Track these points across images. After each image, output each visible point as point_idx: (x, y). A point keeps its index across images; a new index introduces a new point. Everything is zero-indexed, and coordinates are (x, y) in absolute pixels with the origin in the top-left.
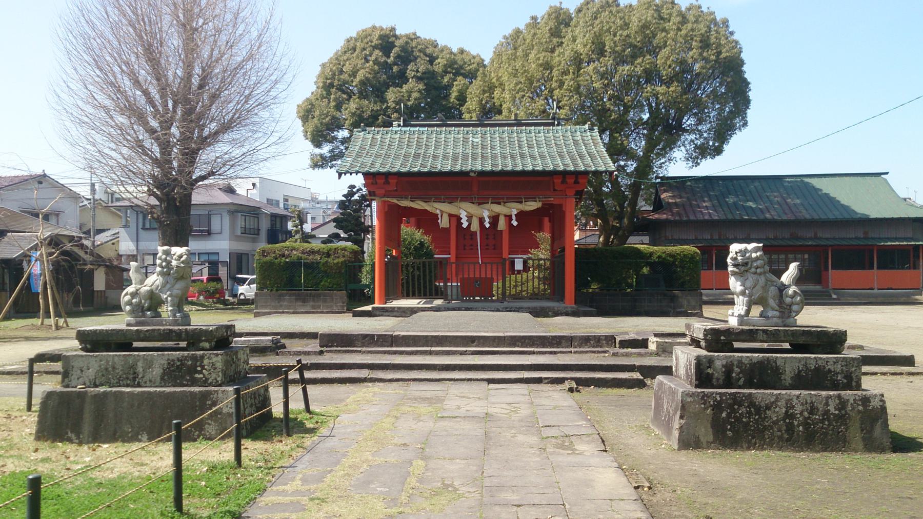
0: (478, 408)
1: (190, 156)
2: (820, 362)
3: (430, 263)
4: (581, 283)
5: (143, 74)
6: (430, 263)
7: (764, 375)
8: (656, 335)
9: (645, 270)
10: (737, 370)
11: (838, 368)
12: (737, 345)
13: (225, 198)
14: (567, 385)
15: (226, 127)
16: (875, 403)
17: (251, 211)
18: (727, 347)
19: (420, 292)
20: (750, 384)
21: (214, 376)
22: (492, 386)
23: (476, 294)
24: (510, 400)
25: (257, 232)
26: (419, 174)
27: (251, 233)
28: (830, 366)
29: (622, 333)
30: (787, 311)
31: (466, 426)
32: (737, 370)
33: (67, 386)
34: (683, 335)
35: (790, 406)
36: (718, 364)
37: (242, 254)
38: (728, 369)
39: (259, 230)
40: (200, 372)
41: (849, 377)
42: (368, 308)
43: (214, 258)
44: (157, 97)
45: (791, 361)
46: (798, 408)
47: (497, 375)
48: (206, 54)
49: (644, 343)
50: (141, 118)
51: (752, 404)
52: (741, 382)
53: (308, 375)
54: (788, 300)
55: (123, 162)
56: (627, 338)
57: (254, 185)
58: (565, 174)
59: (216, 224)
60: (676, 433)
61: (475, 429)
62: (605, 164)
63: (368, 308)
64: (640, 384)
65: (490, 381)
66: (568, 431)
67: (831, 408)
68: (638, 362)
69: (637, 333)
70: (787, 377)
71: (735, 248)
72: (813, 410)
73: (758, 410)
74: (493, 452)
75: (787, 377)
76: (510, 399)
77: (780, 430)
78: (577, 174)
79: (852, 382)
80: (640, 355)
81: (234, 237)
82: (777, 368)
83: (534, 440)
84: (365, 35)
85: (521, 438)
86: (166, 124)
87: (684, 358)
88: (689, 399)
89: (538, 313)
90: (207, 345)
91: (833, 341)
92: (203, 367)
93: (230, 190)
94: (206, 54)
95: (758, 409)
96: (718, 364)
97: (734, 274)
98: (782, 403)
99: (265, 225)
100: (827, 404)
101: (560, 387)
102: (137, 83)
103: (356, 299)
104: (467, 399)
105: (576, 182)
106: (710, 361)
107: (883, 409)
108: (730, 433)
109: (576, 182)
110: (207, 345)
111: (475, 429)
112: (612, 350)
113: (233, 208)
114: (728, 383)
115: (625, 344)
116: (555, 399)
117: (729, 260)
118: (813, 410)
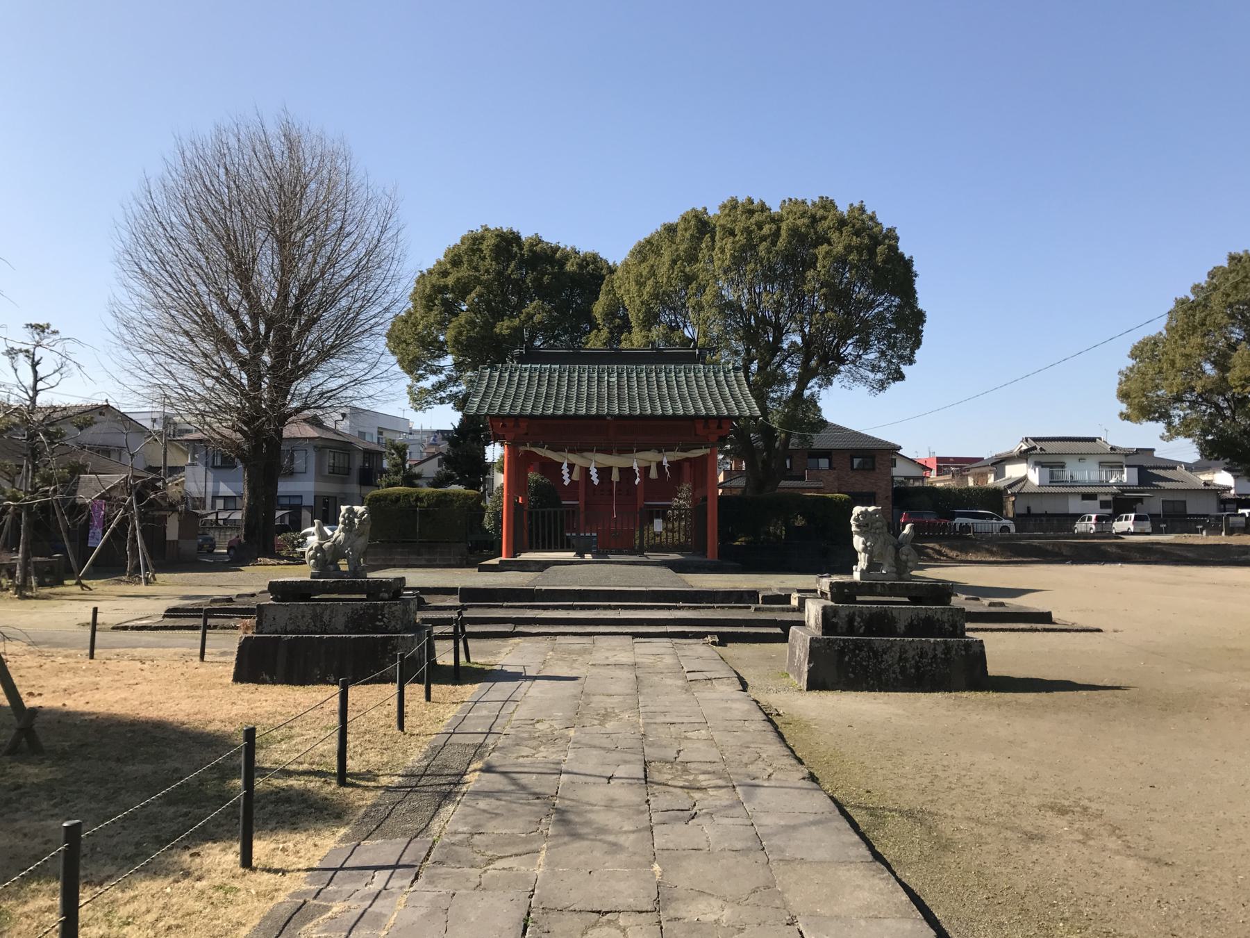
0: (625, 657)
1: (282, 386)
2: (929, 613)
3: (555, 513)
4: (726, 536)
5: (234, 297)
6: (555, 513)
7: (881, 623)
8: (799, 591)
9: (800, 522)
10: (858, 619)
11: (945, 618)
12: (859, 598)
13: (310, 432)
14: (709, 639)
15: (326, 354)
16: (976, 649)
17: (343, 447)
18: (850, 599)
19: (556, 544)
20: (869, 632)
21: (393, 623)
22: (637, 640)
23: (607, 546)
24: (656, 652)
25: (348, 471)
26: (553, 417)
27: (340, 473)
28: (938, 616)
29: (766, 589)
30: (901, 568)
31: (618, 673)
32: (858, 619)
33: (261, 633)
34: (815, 591)
35: (903, 651)
36: (843, 614)
37: (328, 497)
38: (851, 619)
39: (349, 469)
40: (381, 620)
41: (954, 626)
42: (495, 561)
43: (297, 502)
44: (249, 324)
45: (903, 609)
46: (911, 654)
47: (641, 631)
48: (303, 272)
49: (786, 599)
50: (230, 346)
51: (871, 649)
52: (862, 631)
53: (468, 629)
54: (904, 558)
55: (204, 393)
56: (770, 593)
57: (344, 415)
58: (708, 418)
59: (299, 463)
60: (805, 676)
61: (628, 675)
62: (750, 409)
63: (495, 561)
64: (783, 638)
65: (635, 635)
66: (709, 675)
67: (939, 653)
68: (780, 617)
69: (780, 589)
70: (901, 627)
71: (857, 510)
72: (922, 654)
73: (876, 653)
74: (645, 691)
75: (901, 627)
76: (655, 651)
77: (894, 672)
78: (720, 419)
79: (959, 632)
80: (783, 610)
81: (320, 476)
82: (893, 618)
83: (680, 683)
84: (474, 242)
85: (669, 681)
86: (258, 349)
87: (813, 610)
88: (817, 645)
89: (678, 567)
90: (386, 595)
91: (942, 592)
92: (383, 616)
93: (316, 422)
94: (303, 272)
95: (876, 654)
96: (843, 614)
97: (858, 533)
98: (896, 649)
99: (358, 461)
100: (935, 649)
101: (701, 641)
102: (223, 301)
103: (477, 549)
104: (615, 651)
105: (719, 427)
106: (835, 611)
107: (983, 654)
108: (851, 675)
109: (719, 427)
110: (386, 595)
111: (628, 675)
112: (753, 606)
113: (321, 443)
114: (851, 630)
115: (769, 599)
116: (699, 653)
117: (852, 522)
118: (922, 654)
